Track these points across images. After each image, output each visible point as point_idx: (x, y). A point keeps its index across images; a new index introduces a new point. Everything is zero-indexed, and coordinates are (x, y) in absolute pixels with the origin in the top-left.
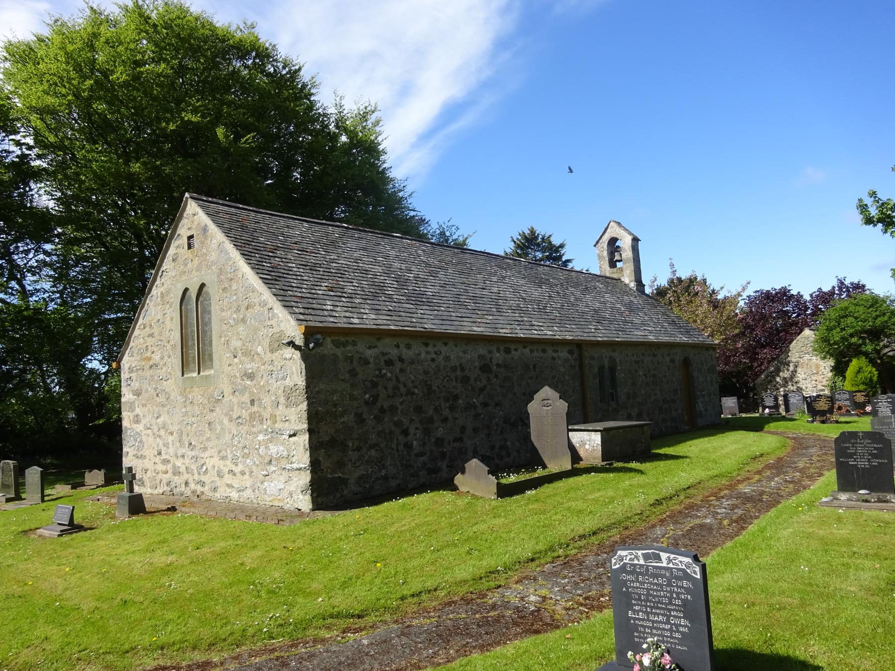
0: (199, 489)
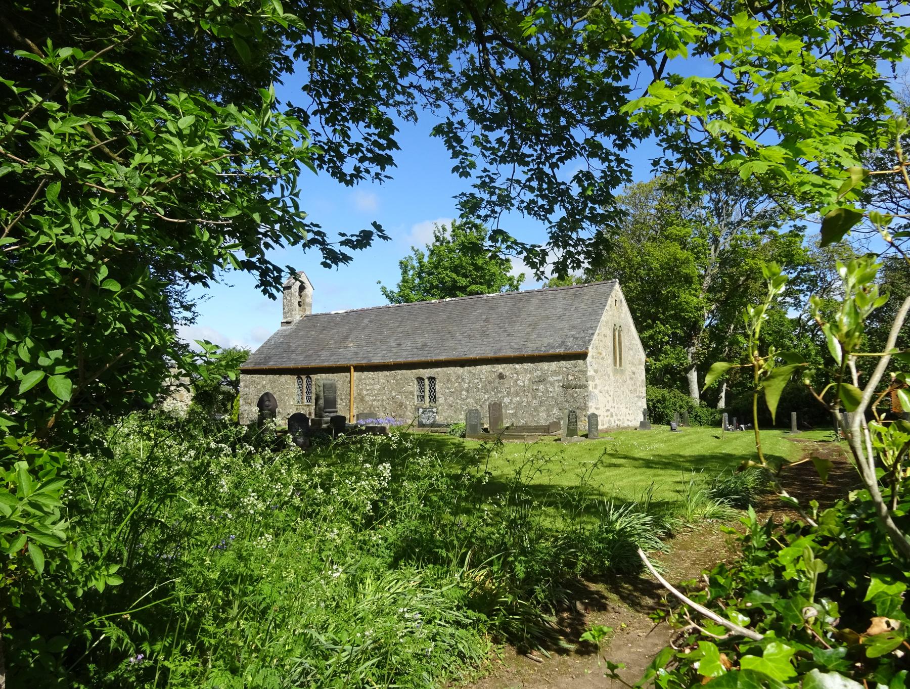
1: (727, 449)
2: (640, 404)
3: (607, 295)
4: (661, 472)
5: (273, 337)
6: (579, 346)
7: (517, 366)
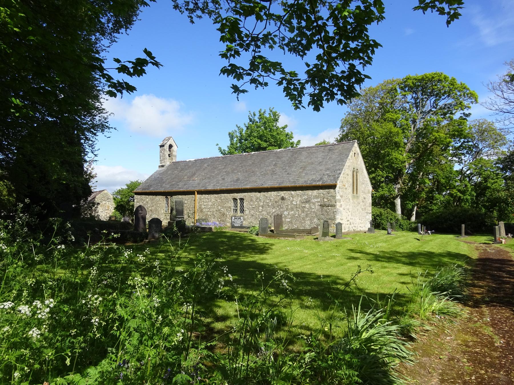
1: (427, 248)
2: (368, 217)
3: (350, 150)
4: (386, 264)
5: (154, 174)
6: (331, 180)
7: (293, 192)
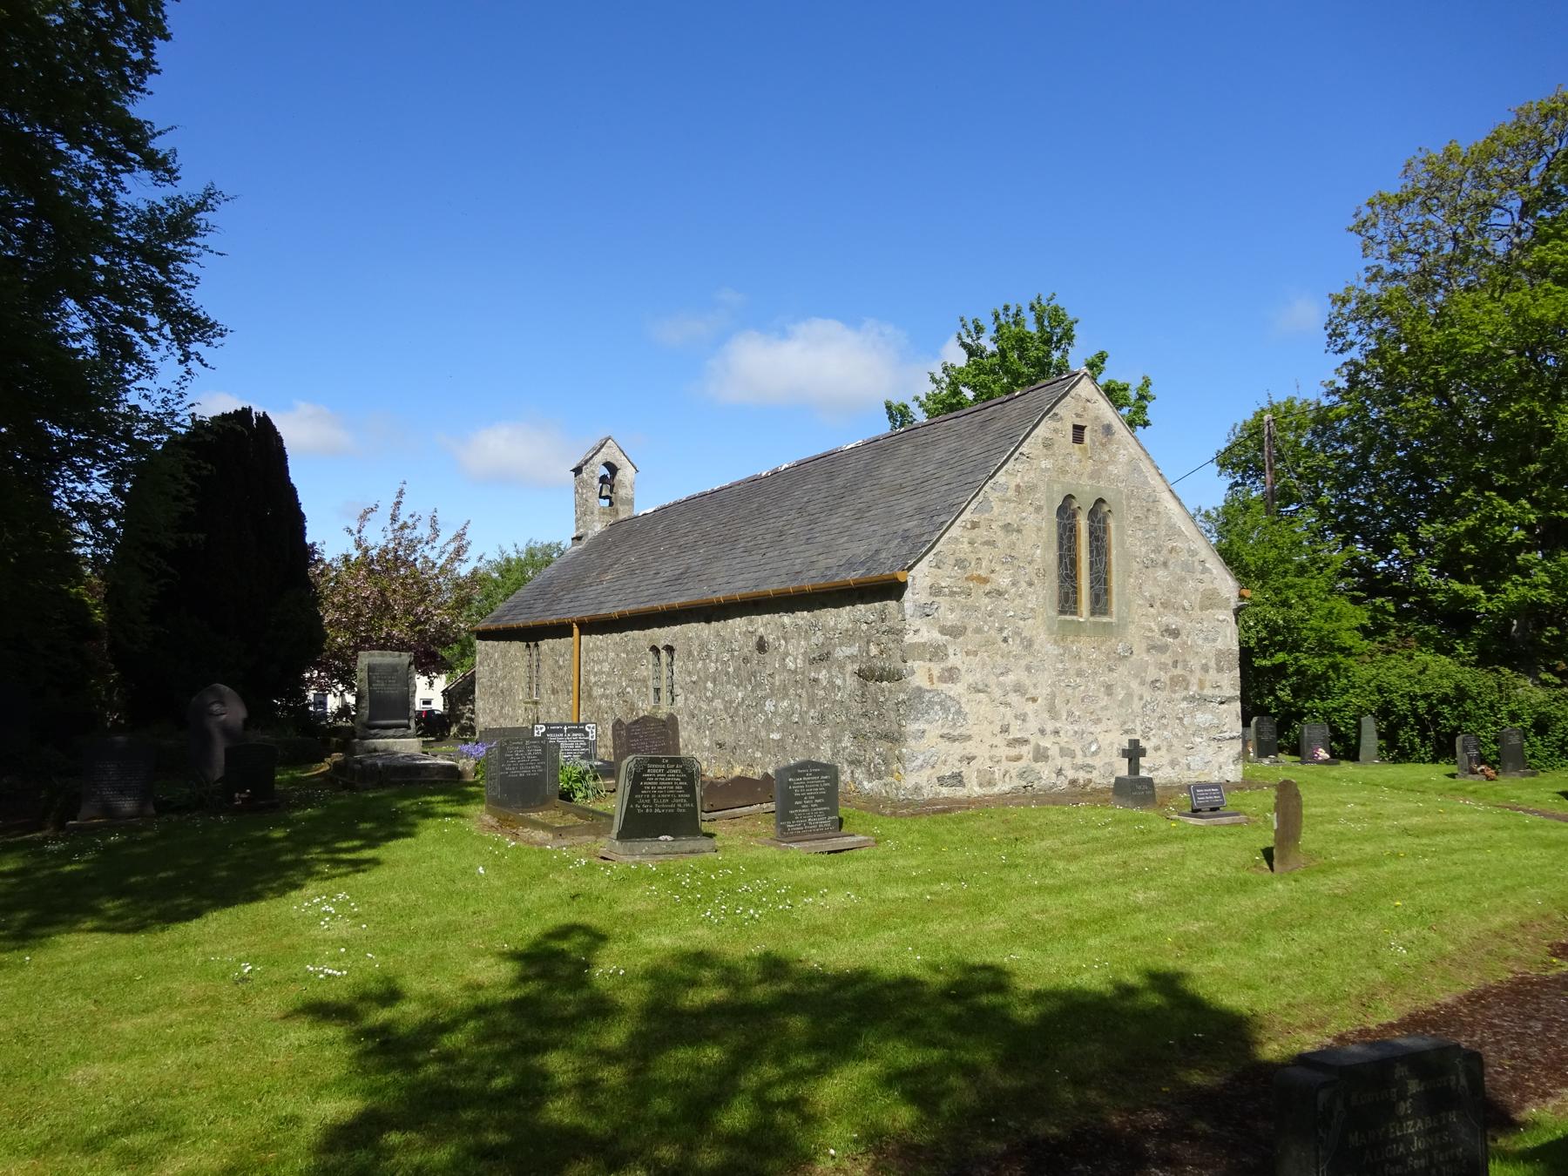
0: (1082, 776)
7: (786, 619)
